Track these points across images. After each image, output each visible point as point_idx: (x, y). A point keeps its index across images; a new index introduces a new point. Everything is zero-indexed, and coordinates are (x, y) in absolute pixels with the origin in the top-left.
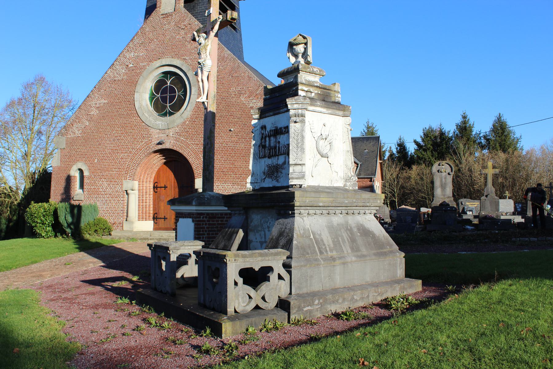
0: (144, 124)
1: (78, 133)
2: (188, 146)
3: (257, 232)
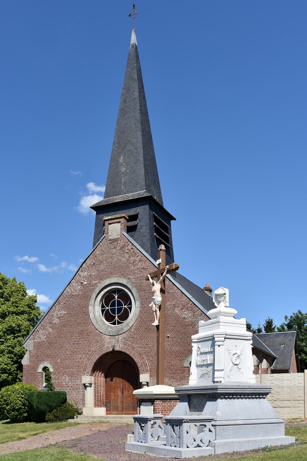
0: (97, 331)
1: (43, 338)
2: (134, 348)
3: (196, 408)
